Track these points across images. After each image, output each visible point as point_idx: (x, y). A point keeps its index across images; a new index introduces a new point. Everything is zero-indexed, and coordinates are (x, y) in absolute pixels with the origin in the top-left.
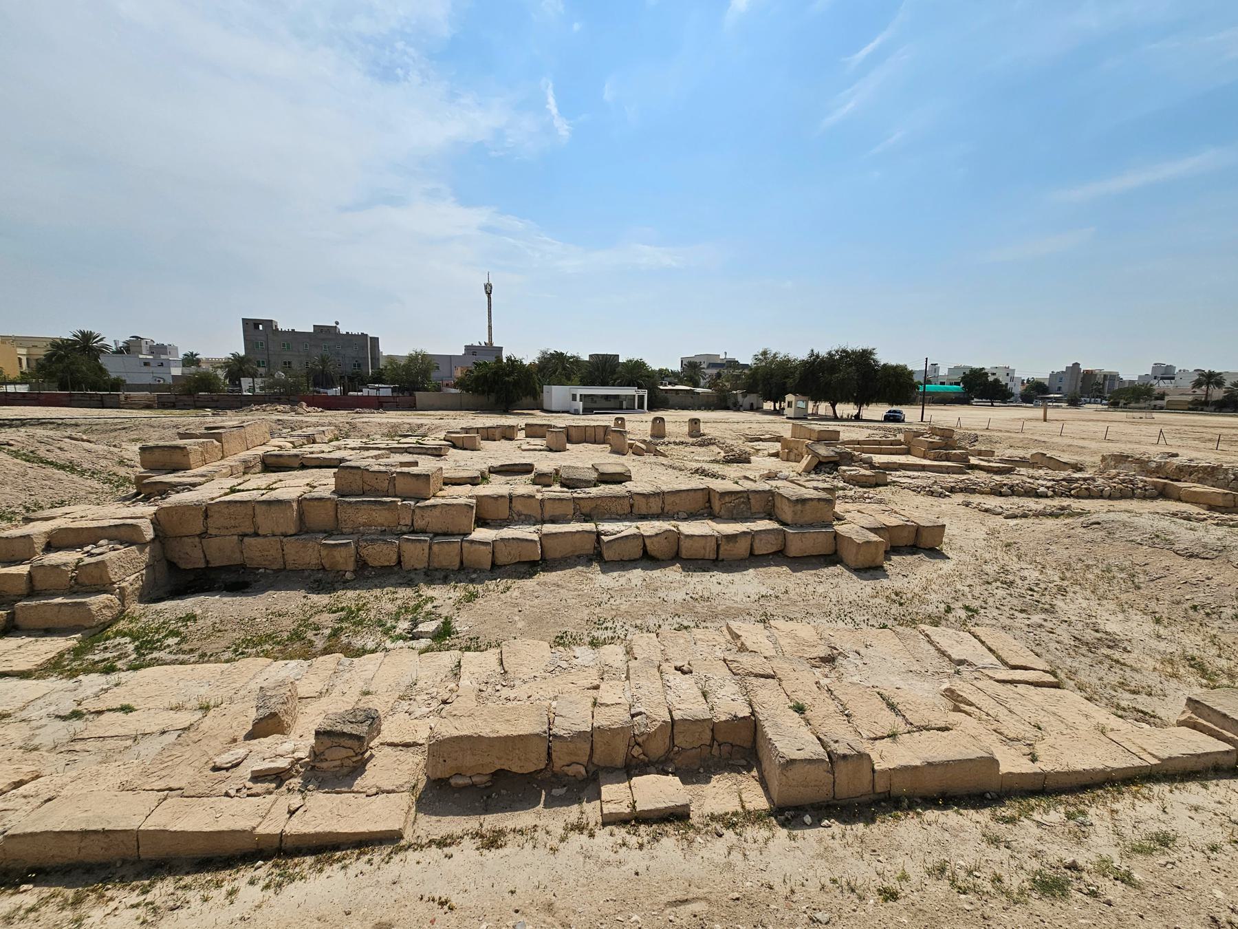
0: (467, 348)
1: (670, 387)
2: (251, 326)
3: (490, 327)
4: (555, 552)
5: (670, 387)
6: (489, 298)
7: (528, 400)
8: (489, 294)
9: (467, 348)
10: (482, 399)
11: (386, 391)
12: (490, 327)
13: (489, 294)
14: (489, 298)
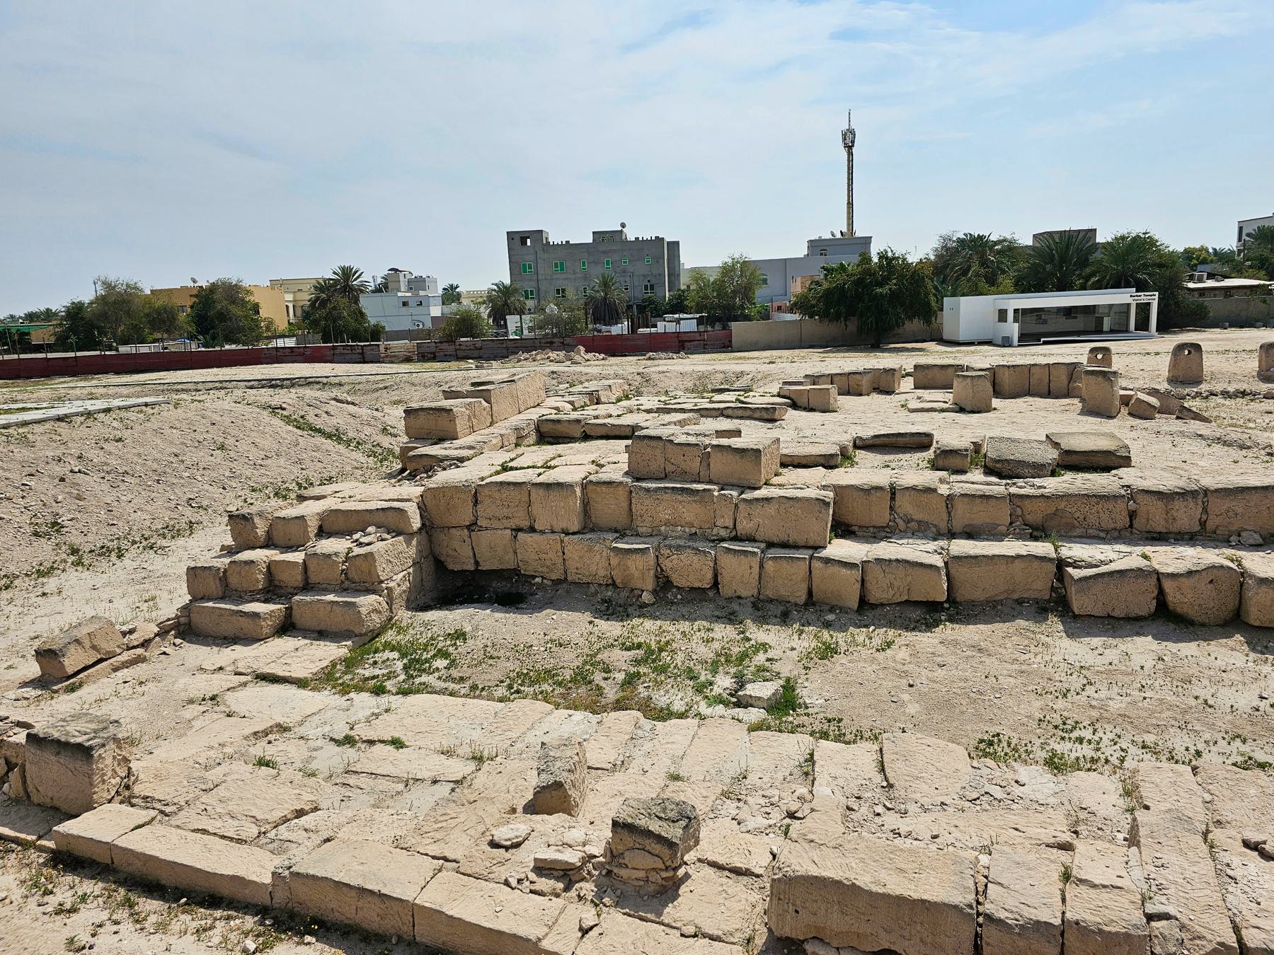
0: (813, 244)
1: (1210, 283)
2: (518, 240)
3: (850, 204)
4: (975, 587)
5: (1210, 283)
6: (850, 154)
7: (915, 325)
8: (849, 148)
9: (813, 244)
10: (832, 329)
11: (688, 324)
12: (850, 204)
13: (849, 148)
14: (850, 154)
